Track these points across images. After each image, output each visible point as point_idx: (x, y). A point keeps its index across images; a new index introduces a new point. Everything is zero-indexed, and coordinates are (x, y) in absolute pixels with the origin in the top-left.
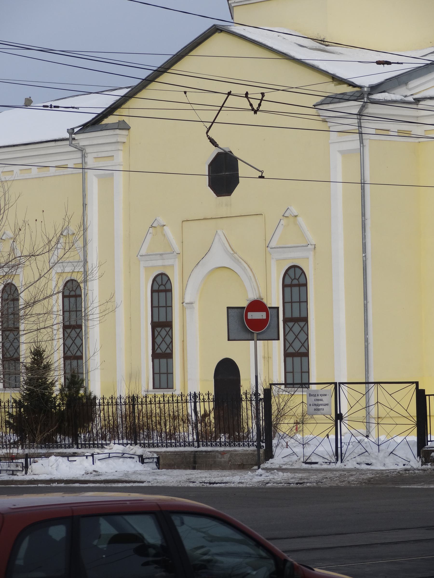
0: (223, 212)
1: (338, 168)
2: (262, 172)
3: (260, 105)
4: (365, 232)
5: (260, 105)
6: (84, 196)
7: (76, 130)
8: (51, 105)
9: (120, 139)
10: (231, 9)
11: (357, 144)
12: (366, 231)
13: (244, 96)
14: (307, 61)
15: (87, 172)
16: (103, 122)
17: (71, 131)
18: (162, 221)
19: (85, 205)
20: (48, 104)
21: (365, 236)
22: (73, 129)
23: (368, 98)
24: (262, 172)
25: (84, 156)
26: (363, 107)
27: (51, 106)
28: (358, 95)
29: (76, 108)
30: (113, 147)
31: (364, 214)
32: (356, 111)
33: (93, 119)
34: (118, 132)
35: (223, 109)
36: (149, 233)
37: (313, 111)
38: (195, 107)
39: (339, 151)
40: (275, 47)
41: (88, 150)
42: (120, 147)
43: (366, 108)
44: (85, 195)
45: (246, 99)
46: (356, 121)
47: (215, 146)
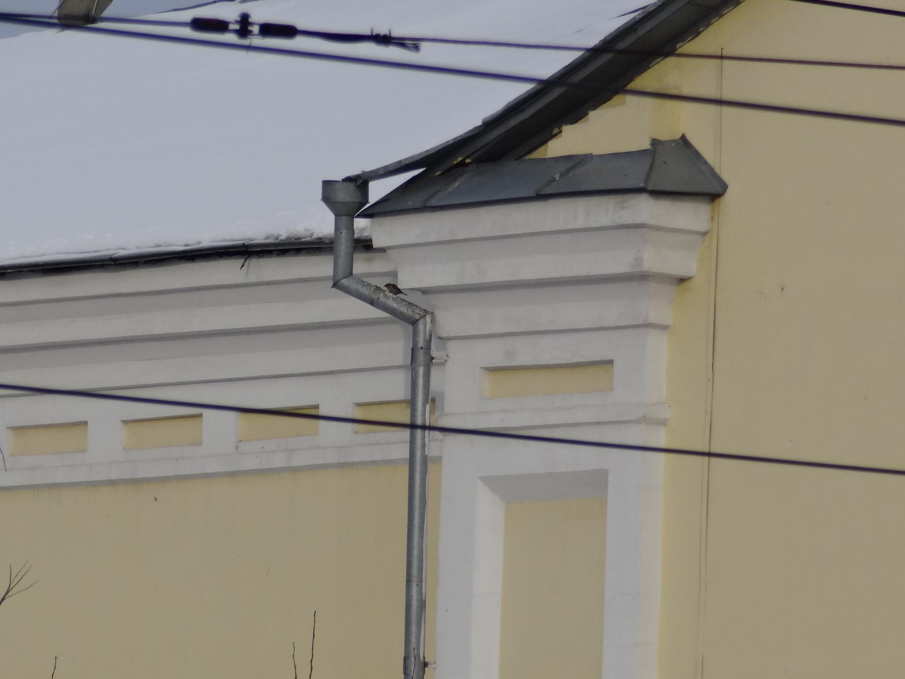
6: (415, 613)
7: (378, 190)
8: (244, 24)
15: (438, 460)
17: (348, 196)
20: (229, 13)
22: (361, 182)
25: (422, 358)
27: (244, 26)
29: (401, 42)
30: (609, 308)
34: (645, 209)
41: (451, 319)
42: (657, 306)
44: (422, 604)
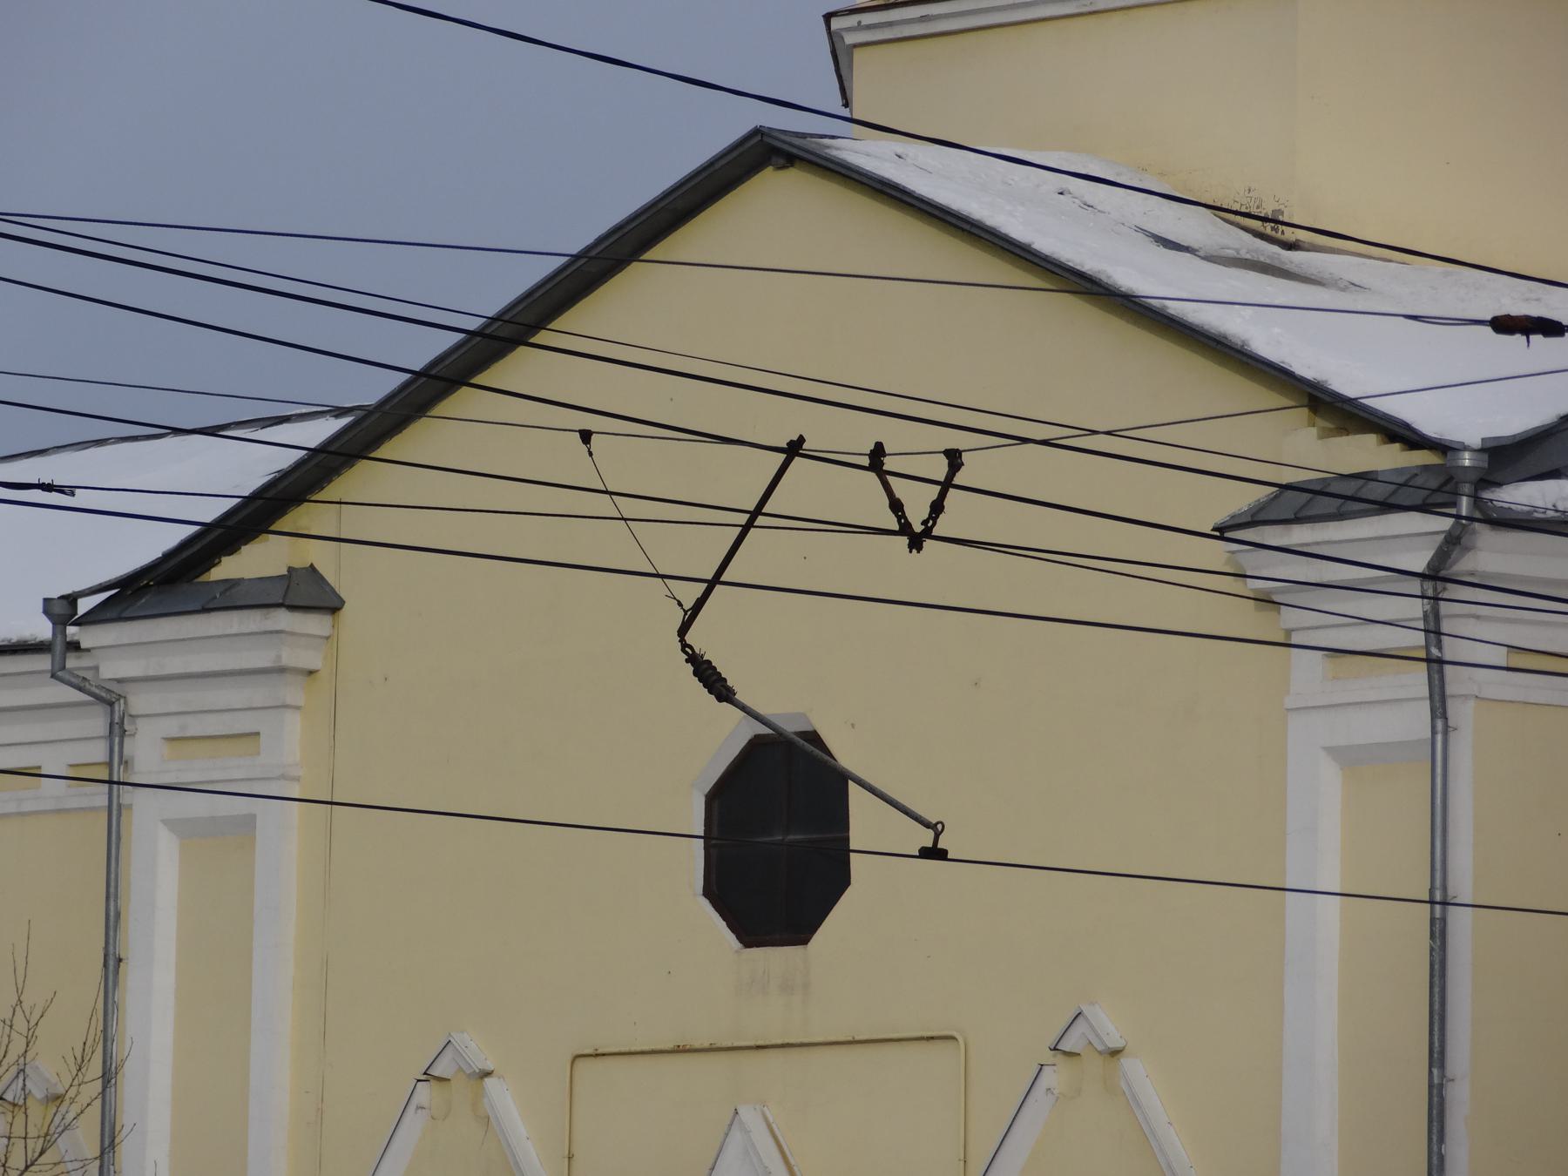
0: (769, 1018)
1: (1325, 827)
2: (937, 829)
3: (937, 508)
4: (1441, 1140)
5: (937, 508)
6: (113, 922)
7: (84, 605)
9: (292, 656)
10: (840, 57)
11: (1415, 721)
12: (1448, 1139)
13: (865, 461)
14: (1174, 308)
15: (130, 807)
16: (217, 573)
17: (62, 610)
18: (478, 1053)
19: (112, 963)
21: (1442, 1158)
22: (71, 600)
23: (1477, 501)
24: (937, 829)
25: (117, 731)
26: (1452, 543)
28: (1434, 484)
29: (60, 490)
30: (257, 693)
31: (1442, 1052)
32: (1418, 561)
33: (168, 556)
34: (283, 619)
35: (760, 520)
36: (412, 1108)
37: (1215, 554)
38: (629, 507)
39: (1332, 751)
40: (1044, 244)
41: (140, 701)
42: (292, 692)
43: (1468, 549)
44: (118, 915)
45: (872, 477)
46: (1414, 609)
47: (720, 699)
